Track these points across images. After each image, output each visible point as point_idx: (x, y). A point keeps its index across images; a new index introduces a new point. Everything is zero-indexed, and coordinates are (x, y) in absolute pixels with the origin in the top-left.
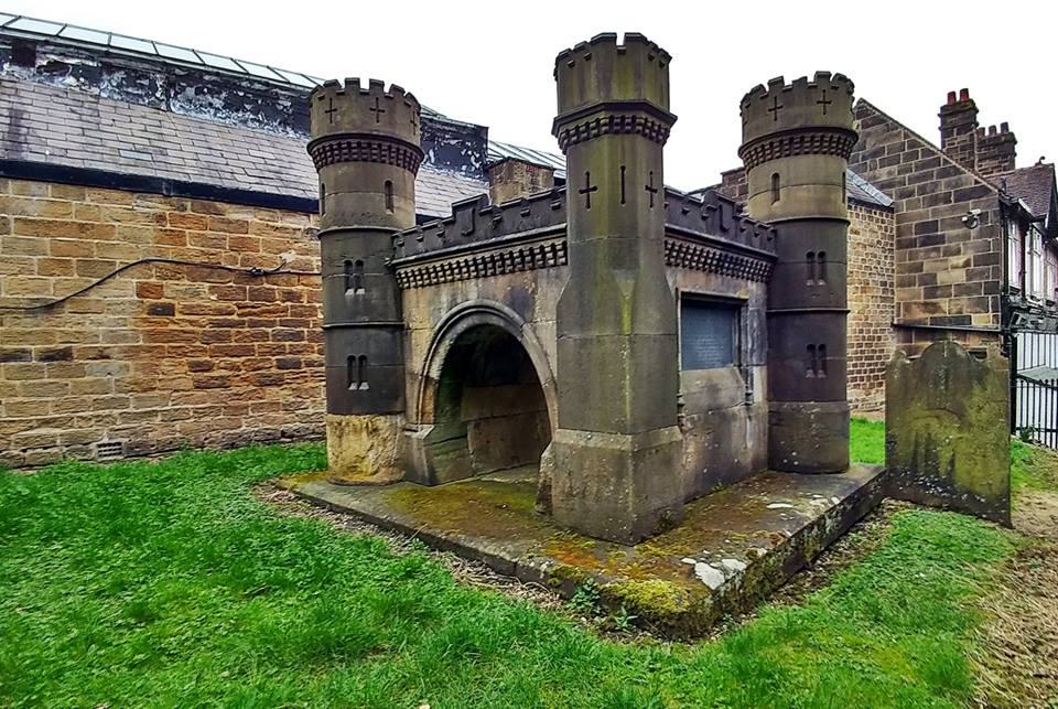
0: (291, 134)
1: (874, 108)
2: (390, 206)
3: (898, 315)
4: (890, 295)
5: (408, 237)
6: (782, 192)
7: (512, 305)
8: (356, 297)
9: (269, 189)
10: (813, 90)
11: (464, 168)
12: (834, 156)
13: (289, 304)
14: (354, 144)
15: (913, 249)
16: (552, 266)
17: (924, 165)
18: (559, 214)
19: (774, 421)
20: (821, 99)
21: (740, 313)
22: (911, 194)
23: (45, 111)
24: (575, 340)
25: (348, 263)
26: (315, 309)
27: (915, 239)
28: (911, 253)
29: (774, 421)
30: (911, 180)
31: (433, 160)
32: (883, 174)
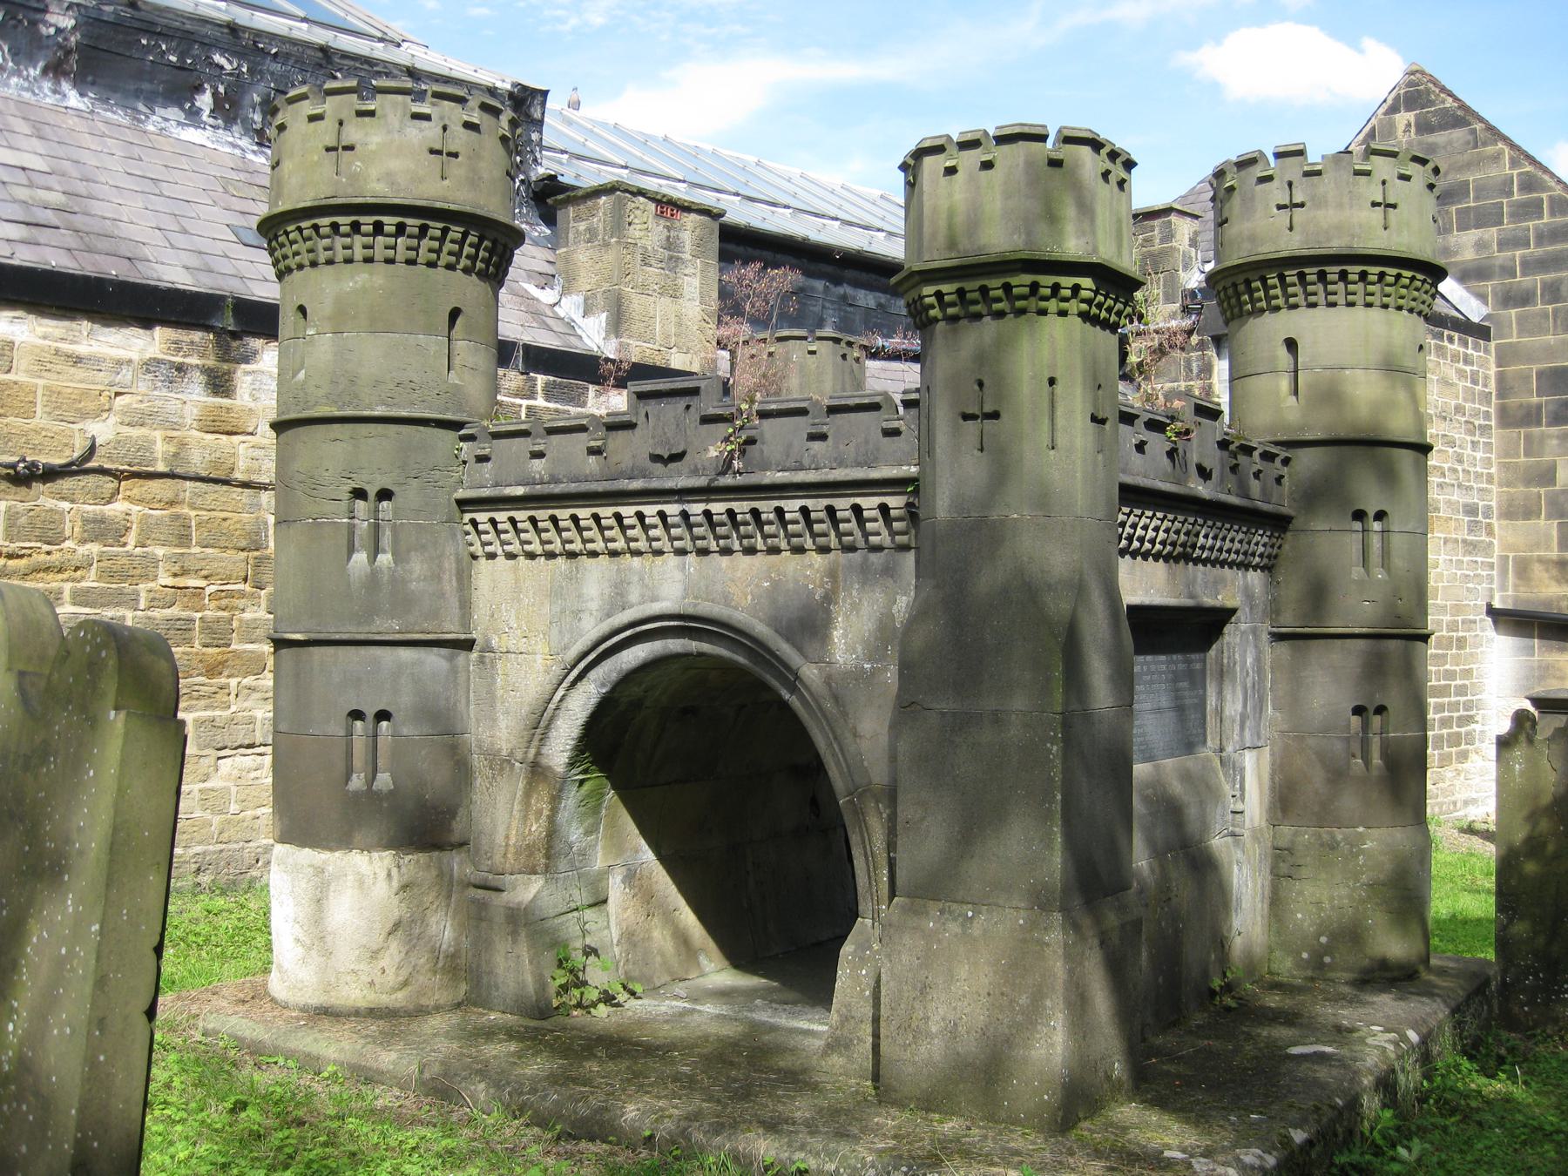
0: (73, 99)
1: (1443, 89)
3: (1503, 588)
9: (53, 258)
10: (1363, 179)
13: (94, 548)
15: (1535, 430)
20: (1379, 199)
22: (1525, 299)
24: (943, 714)
26: (155, 562)
27: (1539, 407)
28: (1528, 438)
29: (1284, 868)
30: (1529, 266)
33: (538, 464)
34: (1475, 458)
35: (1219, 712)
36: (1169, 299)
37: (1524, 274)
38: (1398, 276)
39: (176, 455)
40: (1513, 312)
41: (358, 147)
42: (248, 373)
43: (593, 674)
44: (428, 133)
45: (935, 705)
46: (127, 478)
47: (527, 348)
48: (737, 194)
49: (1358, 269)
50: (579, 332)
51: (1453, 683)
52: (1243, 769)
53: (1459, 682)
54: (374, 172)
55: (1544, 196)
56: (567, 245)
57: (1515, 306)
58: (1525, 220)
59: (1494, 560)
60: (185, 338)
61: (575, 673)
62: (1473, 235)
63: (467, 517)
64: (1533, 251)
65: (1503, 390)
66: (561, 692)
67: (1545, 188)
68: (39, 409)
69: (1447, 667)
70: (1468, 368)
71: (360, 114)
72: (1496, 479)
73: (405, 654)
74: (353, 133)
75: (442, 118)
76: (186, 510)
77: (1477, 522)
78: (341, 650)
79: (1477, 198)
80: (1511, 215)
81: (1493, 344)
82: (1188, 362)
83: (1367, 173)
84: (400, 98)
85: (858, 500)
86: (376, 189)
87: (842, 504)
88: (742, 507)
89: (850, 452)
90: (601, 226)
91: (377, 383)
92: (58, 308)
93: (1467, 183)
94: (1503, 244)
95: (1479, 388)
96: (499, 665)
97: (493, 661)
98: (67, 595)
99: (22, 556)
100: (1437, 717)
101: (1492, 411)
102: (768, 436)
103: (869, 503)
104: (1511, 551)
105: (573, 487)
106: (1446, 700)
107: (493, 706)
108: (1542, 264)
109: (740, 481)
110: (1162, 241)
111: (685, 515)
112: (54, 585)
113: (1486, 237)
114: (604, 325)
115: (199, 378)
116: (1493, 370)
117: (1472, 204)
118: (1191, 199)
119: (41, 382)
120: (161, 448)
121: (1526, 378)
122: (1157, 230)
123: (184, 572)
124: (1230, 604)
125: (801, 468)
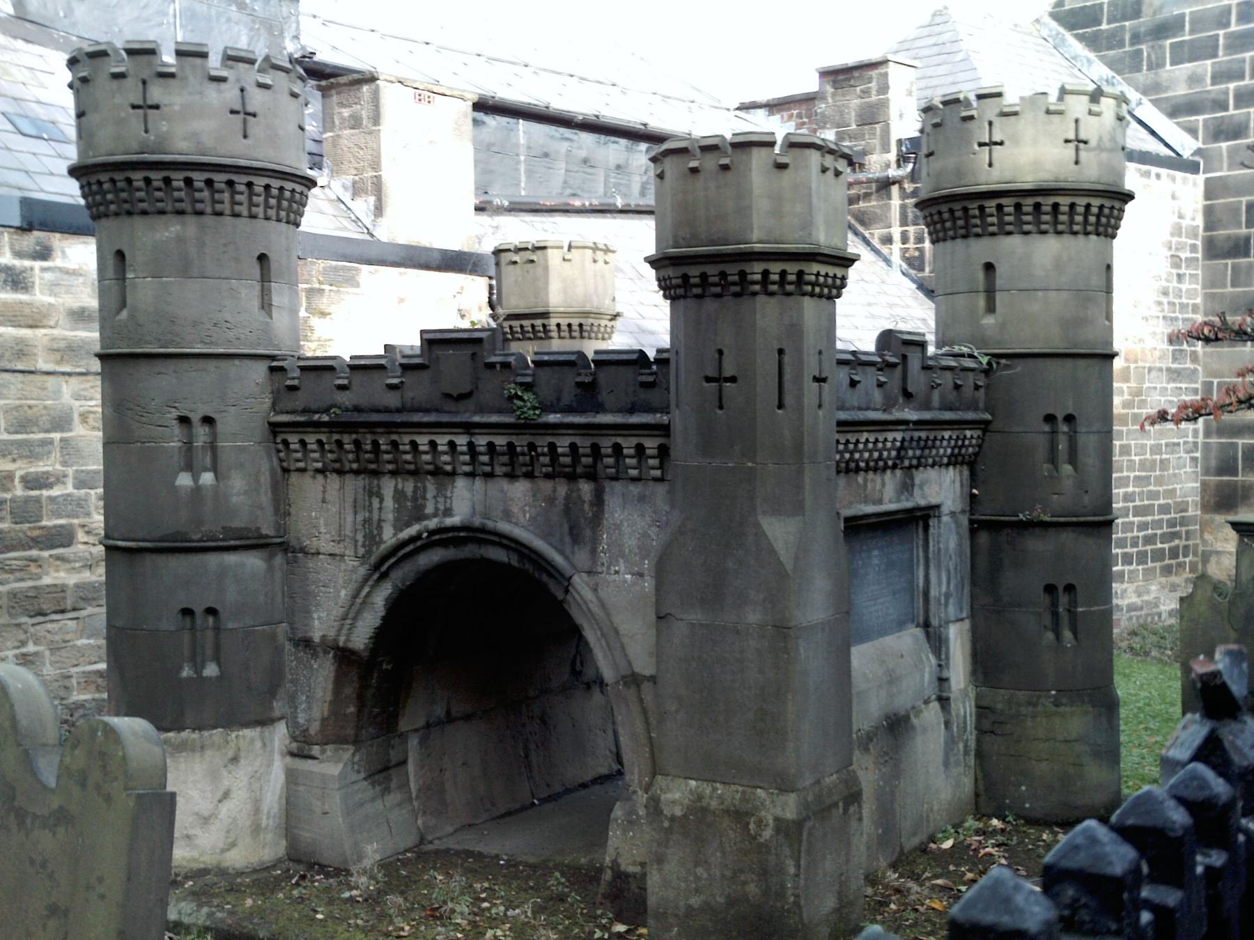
2: (266, 305)
4: (1189, 365)
5: (313, 375)
6: (999, 297)
7: (546, 537)
8: (197, 490)
10: (1056, 118)
16: (634, 480)
18: (654, 396)
19: (834, 292)
20: (1072, 136)
21: (926, 528)
25: (184, 420)
28: (1235, 268)
29: (986, 725)
34: (1180, 290)
35: (926, 594)
37: (1237, 107)
40: (1224, 145)
41: (162, 107)
45: (684, 616)
51: (1156, 503)
52: (947, 640)
53: (1162, 502)
57: (1227, 139)
58: (1242, 52)
59: (1198, 386)
65: (1210, 224)
66: (366, 589)
69: (1151, 488)
72: (1201, 307)
75: (238, 80)
77: (1181, 351)
79: (1192, 32)
93: (1183, 16)
94: (1216, 79)
100: (1141, 534)
101: (1199, 243)
104: (1215, 377)
106: (1149, 518)
111: (471, 445)
113: (1199, 71)
117: (1187, 38)
121: (1235, 210)
124: (934, 501)
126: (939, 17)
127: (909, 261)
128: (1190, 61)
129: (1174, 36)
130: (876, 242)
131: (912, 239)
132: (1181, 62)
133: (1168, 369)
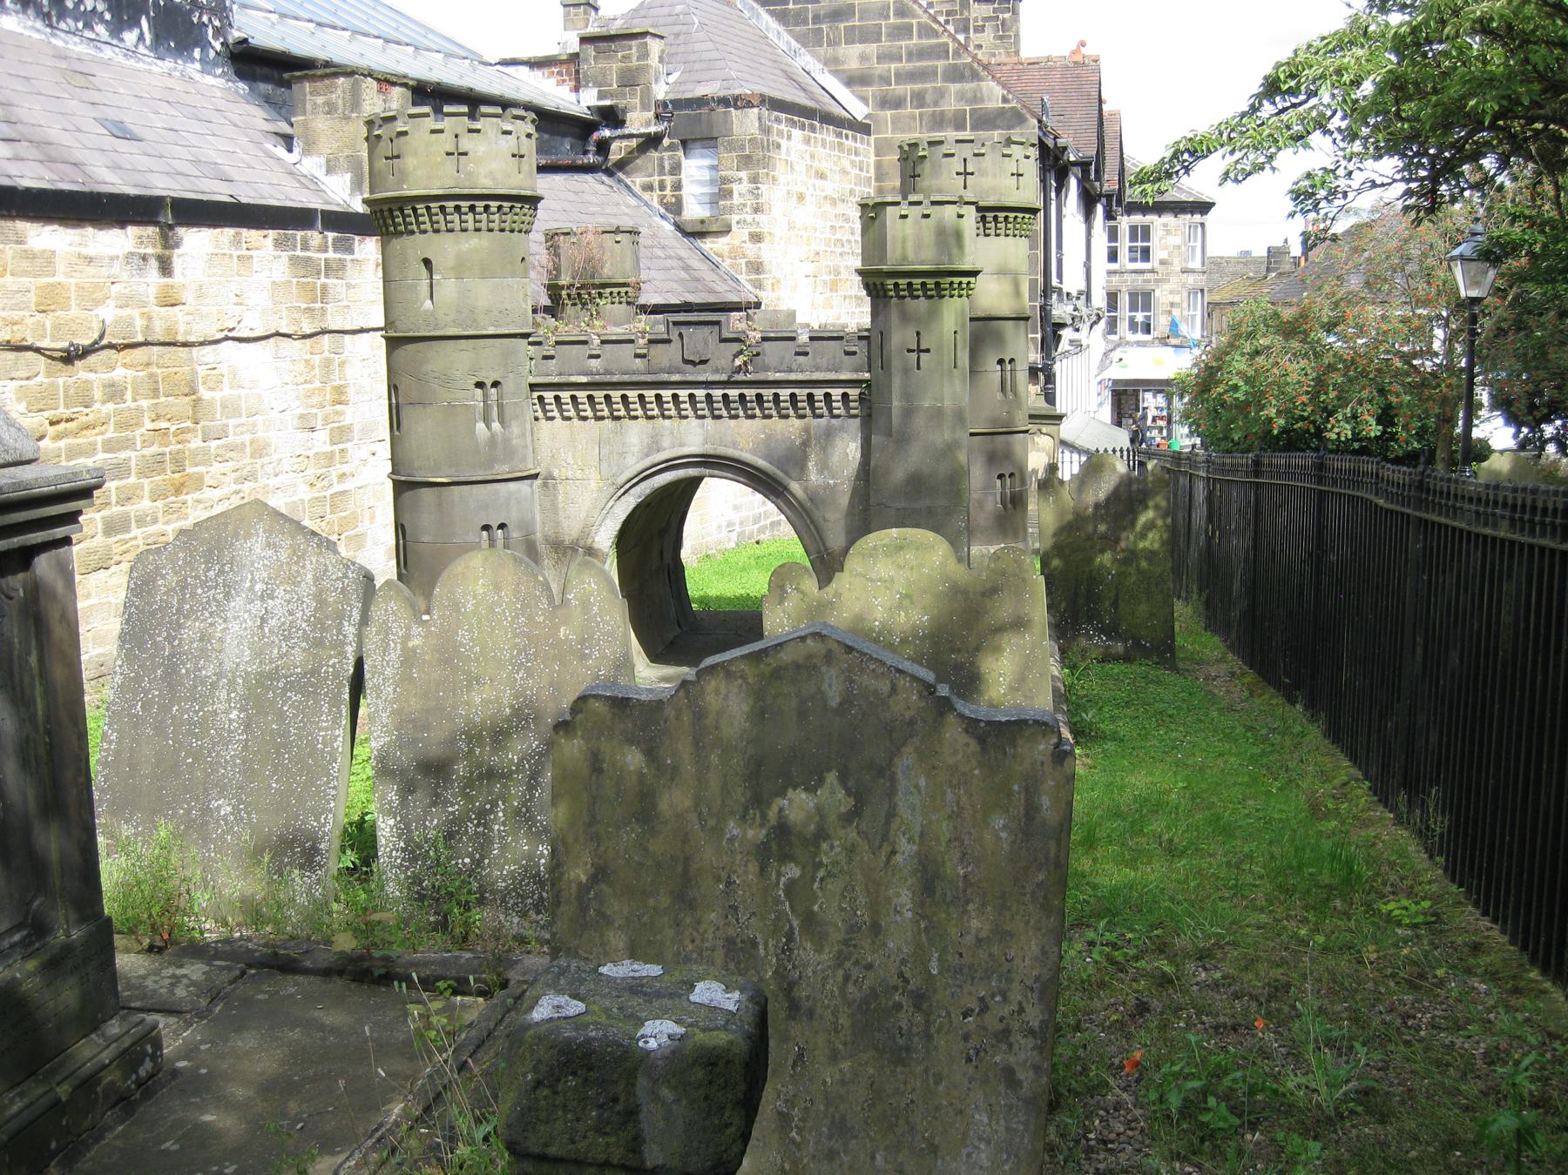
11: (197, 53)
12: (1168, 154)
14: (854, 393)
17: (921, 54)
22: (897, 103)
23: (371, 21)
30: (902, 77)
31: (148, 42)
32: (852, 55)
33: (593, 362)
36: (645, 107)
37: (897, 83)
38: (1016, 218)
39: (147, 327)
40: (889, 113)
41: (470, 154)
42: (179, 256)
43: (632, 491)
44: (508, 144)
46: (122, 349)
47: (322, 211)
48: (311, 21)
49: (1004, 214)
50: (323, 187)
54: (482, 171)
55: (914, 21)
56: (304, 113)
57: (890, 109)
60: (144, 234)
61: (622, 490)
62: (858, 48)
63: (536, 394)
64: (905, 65)
67: (914, 16)
68: (73, 302)
70: (857, 159)
71: (470, 131)
73: (512, 485)
74: (466, 143)
76: (155, 369)
78: (489, 486)
79: (861, 19)
80: (888, 35)
81: (872, 138)
82: (661, 159)
83: (1009, 156)
84: (494, 120)
85: (829, 390)
86: (485, 185)
87: (819, 393)
88: (750, 393)
89: (823, 362)
90: (340, 102)
91: (488, 311)
92: (78, 220)
94: (880, 58)
95: (864, 174)
96: (560, 487)
97: (554, 486)
98: (99, 446)
99: (72, 420)
102: (767, 351)
103: (836, 393)
105: (626, 378)
107: (556, 513)
108: (912, 76)
109: (749, 377)
110: (638, 59)
112: (92, 439)
113: (868, 51)
114: (349, 183)
115: (154, 263)
116: (872, 159)
118: (642, 13)
119: (73, 281)
120: (139, 323)
122: (634, 50)
123: (158, 417)
125: (791, 371)
126: (1213, 204)
127: (667, 207)
128: (861, 42)
129: (847, 21)
130: (637, 189)
131: (669, 188)
132: (853, 42)
133: (856, 297)
